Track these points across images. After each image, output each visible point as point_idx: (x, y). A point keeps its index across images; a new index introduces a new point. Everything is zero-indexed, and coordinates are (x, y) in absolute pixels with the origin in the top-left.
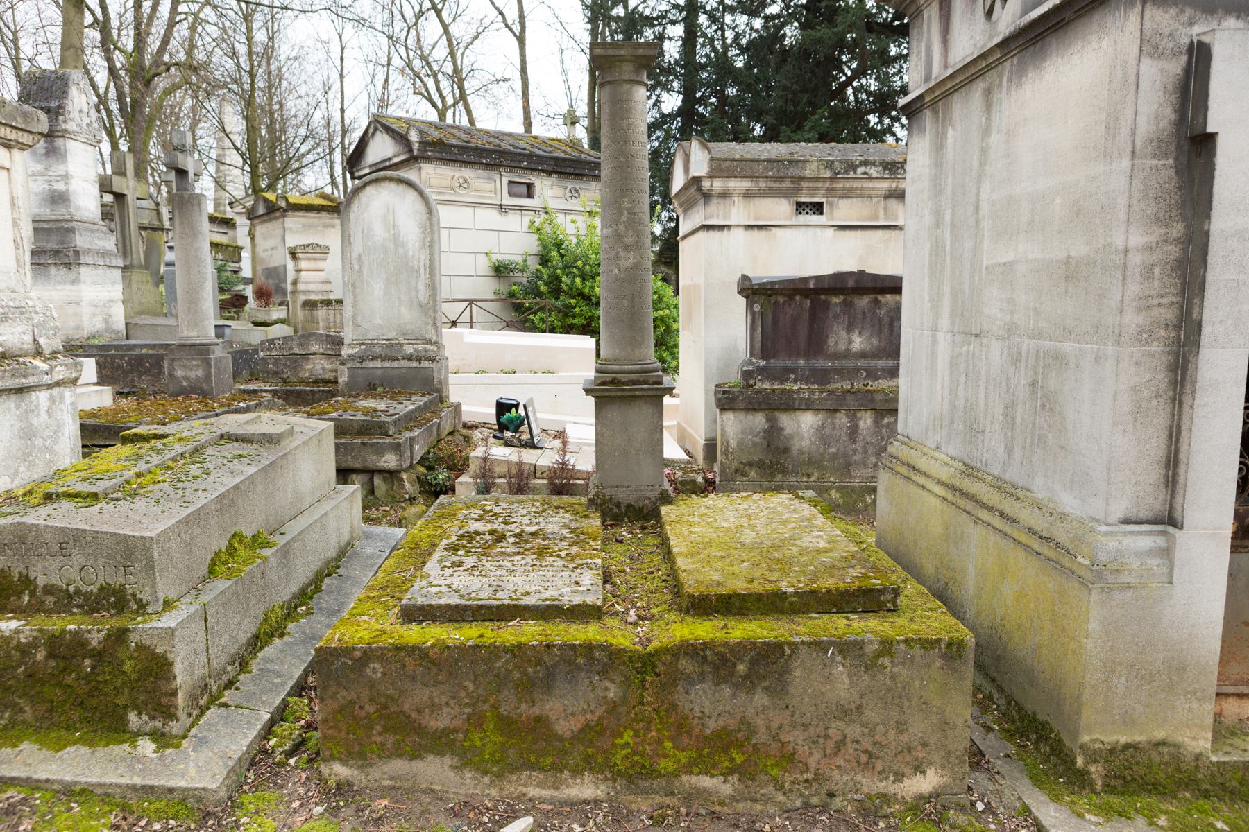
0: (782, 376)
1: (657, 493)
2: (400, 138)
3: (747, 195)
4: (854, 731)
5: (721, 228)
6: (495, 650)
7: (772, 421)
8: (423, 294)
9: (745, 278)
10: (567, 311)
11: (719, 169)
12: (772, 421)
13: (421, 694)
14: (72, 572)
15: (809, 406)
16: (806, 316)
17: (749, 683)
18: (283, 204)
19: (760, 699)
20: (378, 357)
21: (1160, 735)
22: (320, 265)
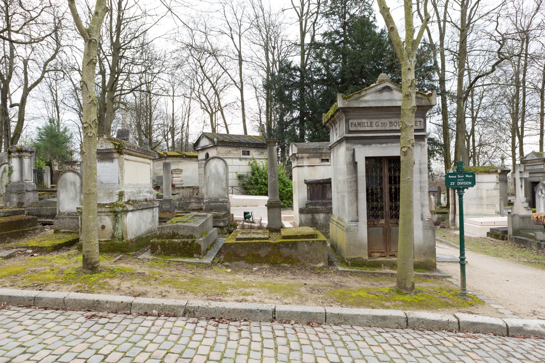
0: (315, 204)
2: (211, 140)
3: (308, 158)
4: (309, 256)
5: (301, 166)
6: (251, 243)
7: (313, 216)
8: (224, 186)
9: (305, 180)
10: (260, 189)
11: (300, 151)
12: (313, 216)
13: (240, 250)
14: (185, 232)
15: (322, 212)
16: (321, 189)
17: (291, 248)
18: (166, 155)
19: (293, 251)
20: (213, 202)
21: (359, 256)
22: (180, 175)
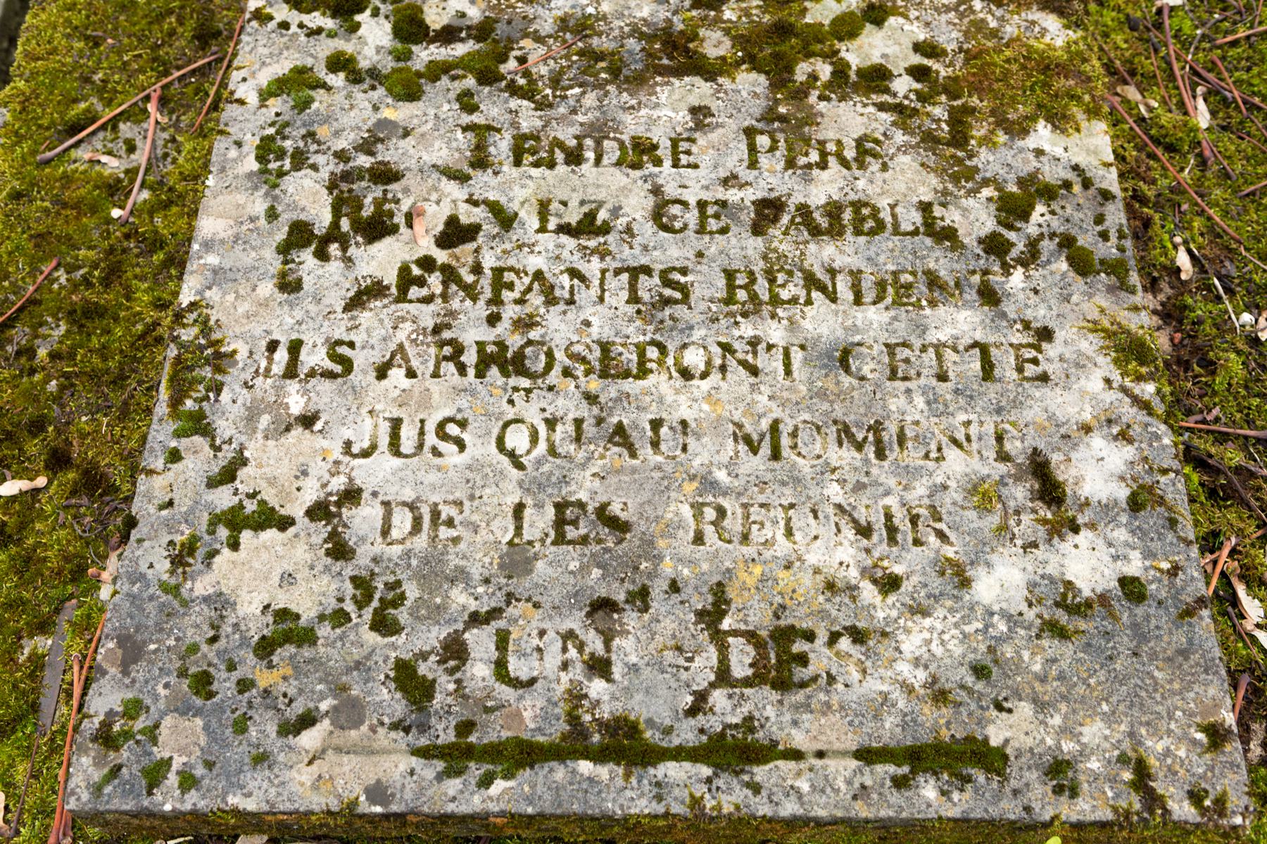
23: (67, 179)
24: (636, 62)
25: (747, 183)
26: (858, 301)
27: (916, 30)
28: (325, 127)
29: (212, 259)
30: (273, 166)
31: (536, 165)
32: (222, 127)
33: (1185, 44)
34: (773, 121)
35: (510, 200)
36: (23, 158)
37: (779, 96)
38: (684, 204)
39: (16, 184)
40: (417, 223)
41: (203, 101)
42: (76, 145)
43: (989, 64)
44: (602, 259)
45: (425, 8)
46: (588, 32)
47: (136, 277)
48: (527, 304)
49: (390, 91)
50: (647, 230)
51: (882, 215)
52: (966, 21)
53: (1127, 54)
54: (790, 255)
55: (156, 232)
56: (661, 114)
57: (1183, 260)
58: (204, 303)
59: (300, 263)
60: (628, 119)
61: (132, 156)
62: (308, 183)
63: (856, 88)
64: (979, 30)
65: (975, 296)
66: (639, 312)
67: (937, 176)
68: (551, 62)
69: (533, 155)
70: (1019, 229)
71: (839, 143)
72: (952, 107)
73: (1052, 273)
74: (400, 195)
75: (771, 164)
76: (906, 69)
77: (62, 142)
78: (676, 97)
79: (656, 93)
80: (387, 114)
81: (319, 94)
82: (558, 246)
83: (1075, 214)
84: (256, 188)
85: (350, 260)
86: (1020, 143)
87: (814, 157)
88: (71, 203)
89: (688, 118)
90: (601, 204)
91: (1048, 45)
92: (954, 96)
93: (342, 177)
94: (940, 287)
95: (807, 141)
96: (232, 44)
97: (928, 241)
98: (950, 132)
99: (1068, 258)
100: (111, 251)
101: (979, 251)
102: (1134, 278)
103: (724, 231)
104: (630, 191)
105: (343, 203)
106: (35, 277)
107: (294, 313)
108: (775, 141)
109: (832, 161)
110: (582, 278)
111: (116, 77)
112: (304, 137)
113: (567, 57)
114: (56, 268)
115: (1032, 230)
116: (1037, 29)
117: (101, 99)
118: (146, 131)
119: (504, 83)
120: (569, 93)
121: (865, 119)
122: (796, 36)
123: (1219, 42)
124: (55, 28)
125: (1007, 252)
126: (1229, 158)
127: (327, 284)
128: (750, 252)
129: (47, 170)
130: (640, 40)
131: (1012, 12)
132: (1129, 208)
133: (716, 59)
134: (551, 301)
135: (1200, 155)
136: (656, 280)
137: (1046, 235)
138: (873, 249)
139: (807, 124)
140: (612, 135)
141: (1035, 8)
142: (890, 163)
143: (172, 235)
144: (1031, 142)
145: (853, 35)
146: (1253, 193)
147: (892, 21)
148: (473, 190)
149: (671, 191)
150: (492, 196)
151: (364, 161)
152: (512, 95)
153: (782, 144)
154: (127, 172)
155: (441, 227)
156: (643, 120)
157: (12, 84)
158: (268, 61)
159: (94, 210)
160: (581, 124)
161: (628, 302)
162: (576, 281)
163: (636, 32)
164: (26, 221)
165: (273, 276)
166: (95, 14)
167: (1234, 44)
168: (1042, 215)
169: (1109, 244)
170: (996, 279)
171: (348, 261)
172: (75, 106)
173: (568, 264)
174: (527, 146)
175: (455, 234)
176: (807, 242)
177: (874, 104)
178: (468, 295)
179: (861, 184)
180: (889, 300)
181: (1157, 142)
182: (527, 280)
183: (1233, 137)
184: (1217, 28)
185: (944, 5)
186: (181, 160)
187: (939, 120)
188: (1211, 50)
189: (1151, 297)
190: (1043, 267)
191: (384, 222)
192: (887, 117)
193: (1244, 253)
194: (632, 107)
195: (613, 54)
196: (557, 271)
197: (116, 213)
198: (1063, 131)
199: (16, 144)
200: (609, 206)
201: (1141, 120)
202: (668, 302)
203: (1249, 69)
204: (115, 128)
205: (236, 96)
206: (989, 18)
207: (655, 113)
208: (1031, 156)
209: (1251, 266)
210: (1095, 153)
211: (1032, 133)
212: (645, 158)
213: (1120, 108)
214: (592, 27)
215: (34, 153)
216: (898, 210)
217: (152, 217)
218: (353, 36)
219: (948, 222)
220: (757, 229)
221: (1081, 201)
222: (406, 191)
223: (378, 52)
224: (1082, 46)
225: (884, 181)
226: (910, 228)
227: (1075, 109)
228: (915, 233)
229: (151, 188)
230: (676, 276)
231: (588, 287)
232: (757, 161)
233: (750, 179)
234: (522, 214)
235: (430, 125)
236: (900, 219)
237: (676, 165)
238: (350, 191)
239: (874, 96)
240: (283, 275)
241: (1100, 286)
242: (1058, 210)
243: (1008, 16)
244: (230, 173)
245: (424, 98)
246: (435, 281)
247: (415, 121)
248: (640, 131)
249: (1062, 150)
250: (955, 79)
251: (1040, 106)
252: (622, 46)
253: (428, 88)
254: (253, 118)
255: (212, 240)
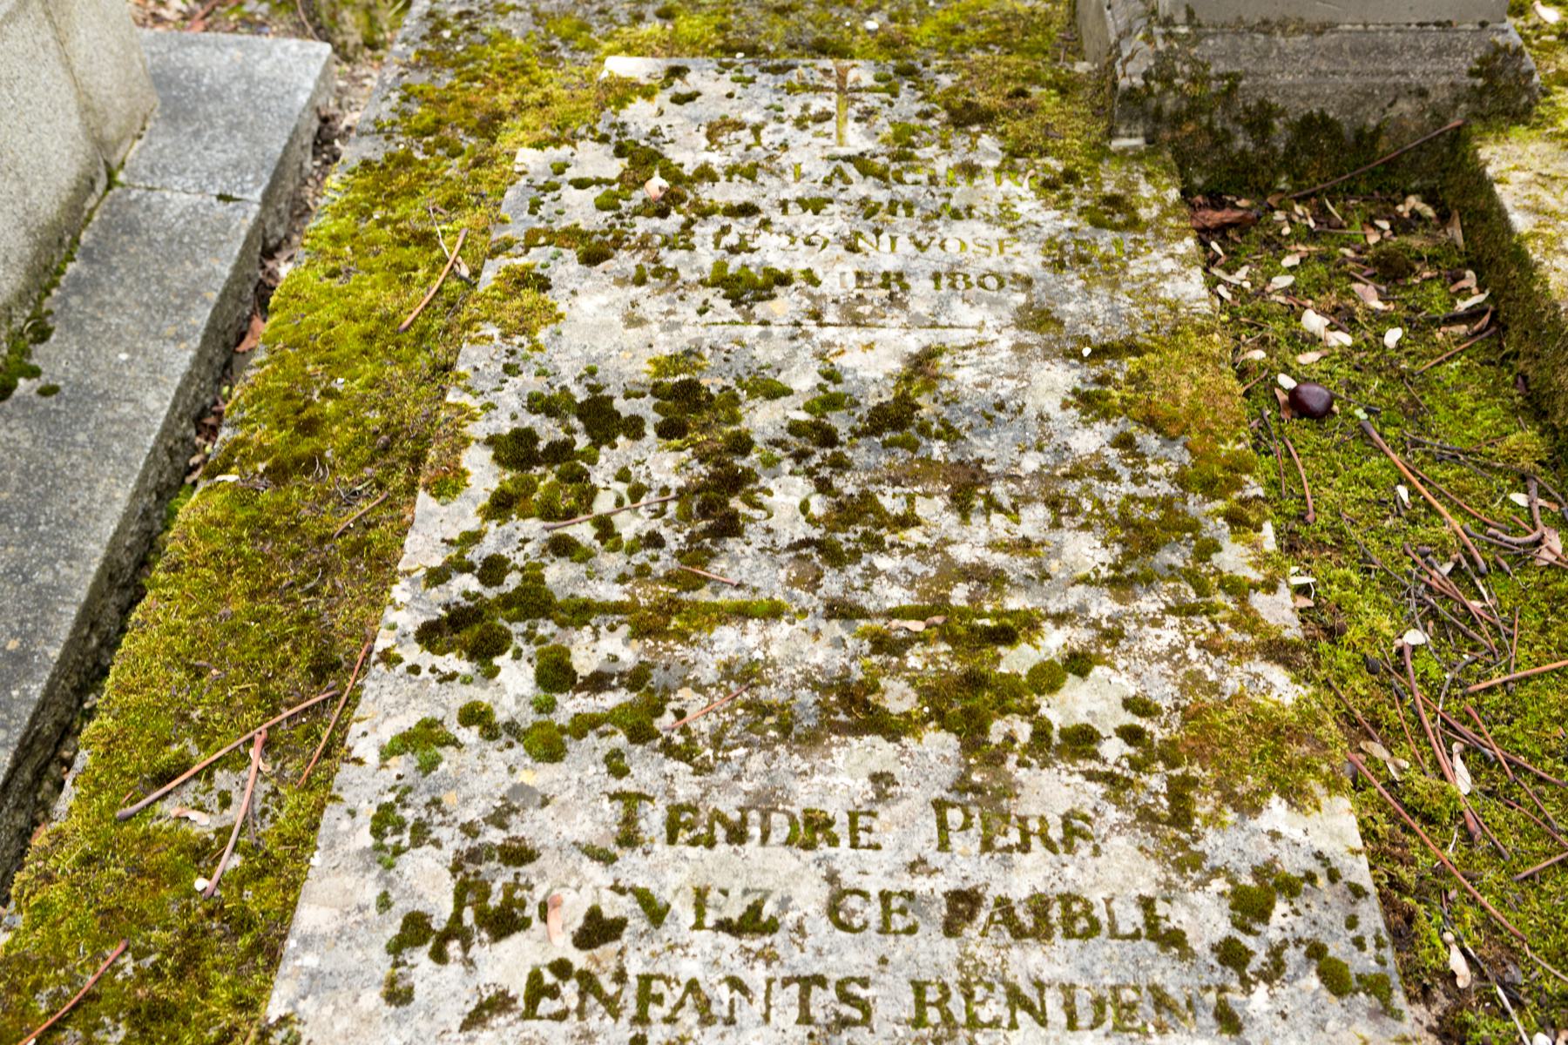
1: (1463, 64)
23: (148, 839)
24: (809, 717)
25: (937, 870)
26: (1072, 1025)
27: (1125, 683)
28: (453, 793)
29: (310, 960)
30: (390, 841)
31: (694, 843)
32: (334, 792)
33: (1434, 690)
34: (965, 791)
35: (662, 888)
36: (101, 814)
37: (972, 761)
38: (864, 895)
39: (88, 845)
40: (551, 915)
41: (313, 746)
42: (163, 797)
43: (1210, 727)
44: (768, 965)
45: (573, 651)
46: (755, 680)
47: (215, 967)
48: (679, 1024)
49: (529, 750)
50: (821, 927)
51: (1095, 913)
52: (1181, 672)
53: (1368, 702)
54: (989, 963)
55: (245, 909)
56: (837, 782)
57: (1457, 963)
58: (295, 1018)
59: (413, 966)
60: (799, 786)
61: (226, 812)
62: (428, 863)
63: (1059, 751)
64: (1196, 683)
65: (1211, 1021)
66: (811, 1036)
67: (1158, 863)
68: (713, 716)
69: (690, 830)
70: (1258, 934)
71: (1043, 819)
72: (1171, 778)
73: (1301, 992)
74: (534, 880)
75: (965, 844)
76: (1116, 730)
77: (147, 794)
78: (855, 760)
79: (831, 756)
80: (525, 777)
81: (448, 753)
82: (717, 948)
83: (1323, 914)
84: (368, 869)
85: (471, 962)
86: (1252, 823)
87: (1014, 837)
88: (150, 870)
89: (869, 786)
90: (767, 894)
91: (1276, 703)
92: (1173, 764)
93: (468, 857)
94: (1170, 1008)
95: (1006, 817)
96: (352, 678)
97: (1152, 947)
98: (1170, 809)
99: (1319, 972)
100: (189, 933)
101: (1213, 961)
102: (1399, 999)
103: (911, 930)
104: (802, 877)
105: (468, 890)
106: (96, 964)
107: (402, 1033)
108: (968, 816)
109: (1035, 842)
110: (744, 990)
111: (218, 715)
112: (427, 805)
113: (731, 710)
114: (122, 954)
115: (1273, 933)
116: (1262, 684)
117: (198, 741)
118: (245, 781)
119: (659, 742)
120: (732, 754)
121: (1071, 791)
122: (990, 688)
123: (1472, 689)
124: (154, 655)
125: (1245, 963)
126: (1499, 830)
127: (442, 994)
128: (942, 958)
129: (126, 828)
130: (813, 690)
131: (1232, 663)
132: (1384, 898)
133: (900, 715)
134: (706, 1020)
135: (1464, 827)
136: (832, 993)
137: (1291, 940)
138: (1088, 956)
139: (1004, 795)
140: (781, 807)
141: (1258, 657)
142: (1102, 847)
143: (263, 913)
144: (1265, 822)
145: (1053, 688)
146: (1532, 876)
147: (1098, 671)
148: (619, 875)
149: (849, 879)
150: (641, 883)
151: (494, 836)
152: (667, 756)
153: (976, 820)
154: (218, 831)
155: (579, 922)
156: (816, 789)
157: (97, 721)
158: (393, 711)
159: (175, 878)
160: (746, 793)
161: (798, 1022)
162: (737, 994)
163: (809, 681)
164: (94, 892)
165: (380, 983)
166: (202, 639)
167: (1490, 690)
168: (1284, 915)
169: (1366, 954)
170: (1235, 997)
171: (469, 963)
172: (167, 749)
173: (727, 972)
174: (683, 819)
175: (597, 930)
176: (1009, 946)
177: (1082, 773)
178: (608, 1010)
179: (1070, 872)
180: (1109, 1024)
181: (1412, 811)
182: (679, 992)
183: (1500, 804)
184: (1468, 671)
185: (1155, 653)
186: (282, 818)
187: (1157, 793)
188: (1464, 696)
189: (1424, 1009)
190: (1290, 983)
191: (514, 915)
192: (1097, 789)
193: (1529, 954)
194: (805, 773)
195: (783, 707)
196: (714, 981)
197: (200, 883)
198: (1301, 809)
199: (91, 796)
200: (776, 896)
201: (1391, 784)
202: (845, 1023)
203: (1510, 722)
204: (209, 777)
205: (354, 754)
206: (1207, 669)
207: (831, 780)
208: (1266, 840)
209: (1539, 971)
210: (1340, 837)
211: (1265, 811)
212: (819, 836)
213: (1364, 769)
214: (759, 675)
215: (113, 806)
216: (1115, 906)
217: (242, 890)
218: (491, 682)
219: (1173, 924)
220: (950, 930)
221: (1329, 898)
222: (542, 874)
223: (518, 702)
224: (1315, 706)
225: (1097, 869)
226: (1130, 930)
227: (1312, 782)
228: (1136, 936)
229: (244, 853)
230: (855, 989)
231: (750, 1001)
232: (948, 842)
233: (941, 864)
234: (675, 906)
235: (572, 792)
236: (1117, 918)
237: (854, 846)
238: (477, 874)
239: (1080, 762)
240: (392, 982)
241: (1359, 1010)
242: (1303, 910)
243: (1228, 667)
244: (339, 849)
245: (567, 759)
246: (570, 990)
247: (556, 787)
248: (814, 803)
249: (1301, 833)
250: (1172, 743)
251: (1271, 778)
252: (793, 698)
253: (572, 746)
254: (371, 781)
255: (312, 935)
